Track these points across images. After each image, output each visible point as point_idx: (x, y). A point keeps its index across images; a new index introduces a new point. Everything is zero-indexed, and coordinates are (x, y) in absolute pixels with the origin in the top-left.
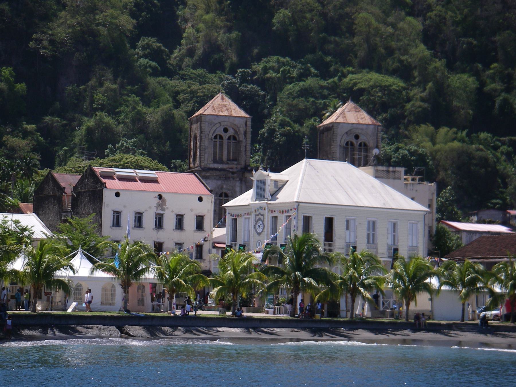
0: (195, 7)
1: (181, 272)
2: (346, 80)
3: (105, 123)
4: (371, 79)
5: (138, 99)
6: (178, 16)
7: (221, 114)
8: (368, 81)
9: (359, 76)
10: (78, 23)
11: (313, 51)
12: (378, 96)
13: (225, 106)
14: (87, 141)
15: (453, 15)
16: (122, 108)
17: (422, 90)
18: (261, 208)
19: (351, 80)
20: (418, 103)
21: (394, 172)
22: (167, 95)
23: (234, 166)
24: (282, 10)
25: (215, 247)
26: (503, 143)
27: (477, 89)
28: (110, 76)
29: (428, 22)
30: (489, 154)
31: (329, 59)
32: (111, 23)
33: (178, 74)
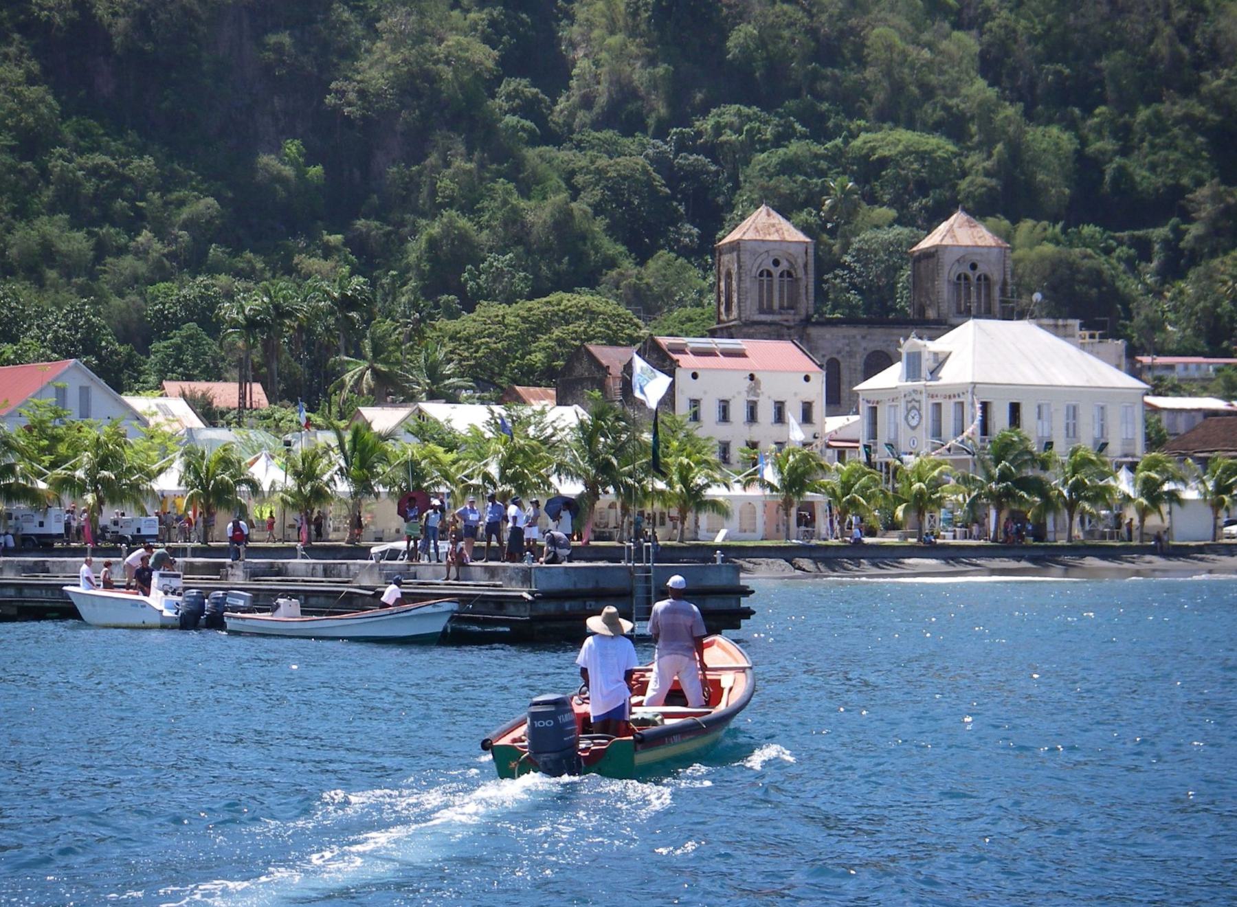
0: (591, 25)
1: (857, 486)
2: (857, 143)
3: (458, 228)
4: (900, 141)
5: (511, 186)
6: (560, 39)
7: (768, 238)
8: (896, 143)
9: (879, 135)
10: (405, 61)
11: (796, 94)
12: (913, 170)
13: (774, 225)
14: (429, 260)
15: (1029, 25)
16: (486, 204)
17: (985, 156)
18: (915, 391)
19: (865, 143)
20: (981, 180)
21: (1065, 326)
22: (555, 176)
23: (791, 318)
24: (743, 27)
25: (829, 446)
26: (1121, 243)
27: (1076, 151)
28: (462, 149)
29: (986, 38)
30: (1101, 262)
31: (825, 106)
32: (459, 59)
33: (571, 140)
